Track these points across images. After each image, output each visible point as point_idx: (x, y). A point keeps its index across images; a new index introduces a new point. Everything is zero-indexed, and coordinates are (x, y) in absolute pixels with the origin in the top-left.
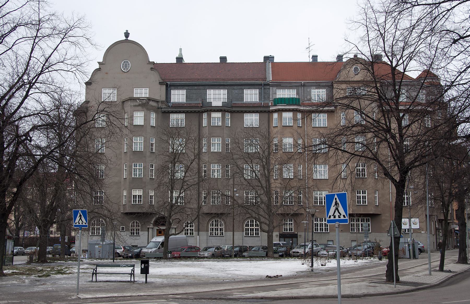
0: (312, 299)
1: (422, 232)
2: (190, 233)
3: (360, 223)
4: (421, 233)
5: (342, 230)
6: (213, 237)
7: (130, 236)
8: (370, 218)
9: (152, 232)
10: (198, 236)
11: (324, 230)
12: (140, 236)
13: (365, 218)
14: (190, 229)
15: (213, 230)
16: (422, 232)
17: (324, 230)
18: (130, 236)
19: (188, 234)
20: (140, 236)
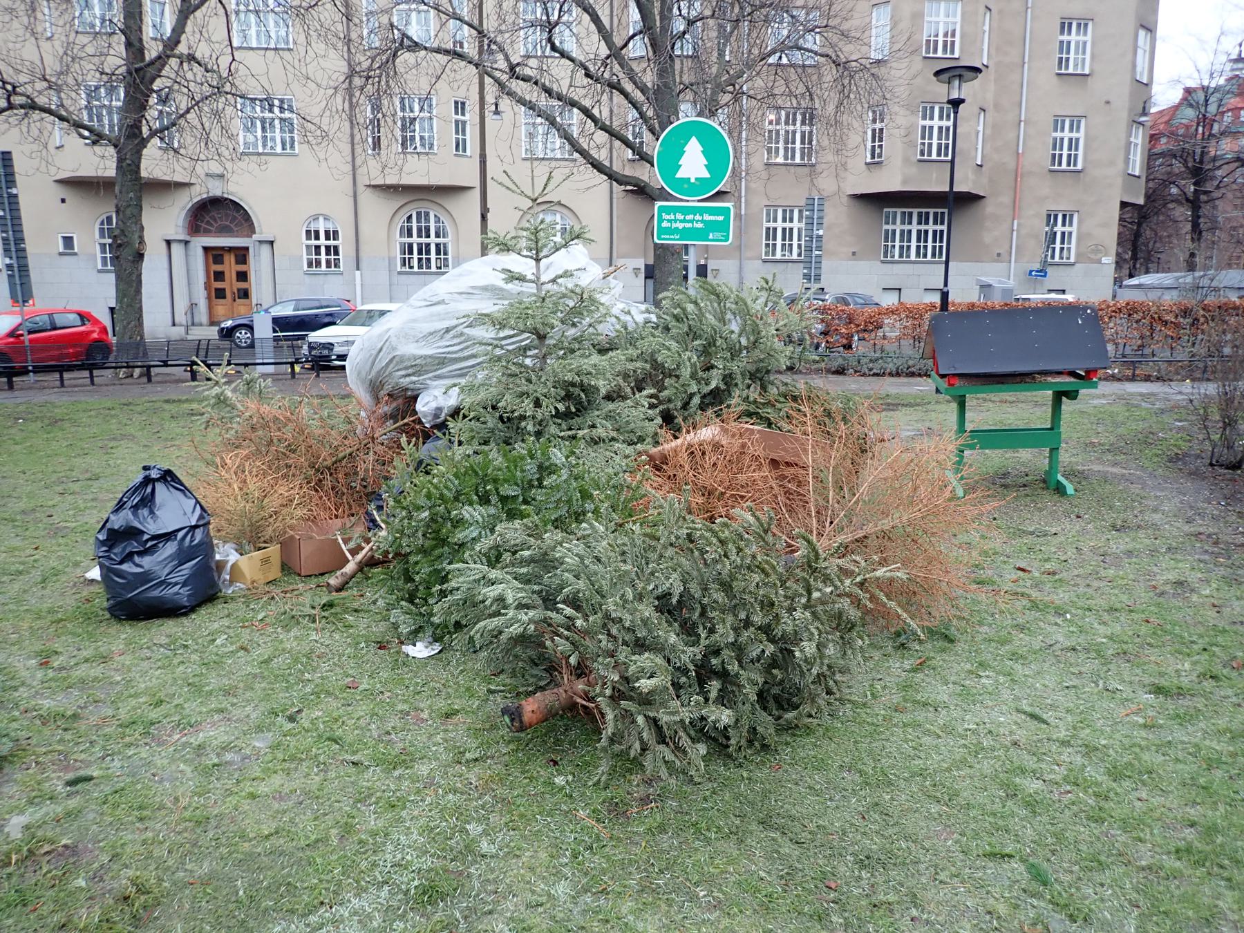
0: (203, 611)
1: (1104, 260)
2: (328, 262)
3: (914, 228)
4: (1099, 262)
5: (854, 254)
6: (411, 276)
7: (99, 271)
8: (946, 211)
9: (183, 257)
10: (358, 273)
11: (798, 155)
12: (76, 254)
13: (932, 211)
14: (328, 248)
15: (411, 252)
16: (1104, 260)
17: (798, 155)
18: (99, 271)
19: (318, 263)
20: (76, 254)
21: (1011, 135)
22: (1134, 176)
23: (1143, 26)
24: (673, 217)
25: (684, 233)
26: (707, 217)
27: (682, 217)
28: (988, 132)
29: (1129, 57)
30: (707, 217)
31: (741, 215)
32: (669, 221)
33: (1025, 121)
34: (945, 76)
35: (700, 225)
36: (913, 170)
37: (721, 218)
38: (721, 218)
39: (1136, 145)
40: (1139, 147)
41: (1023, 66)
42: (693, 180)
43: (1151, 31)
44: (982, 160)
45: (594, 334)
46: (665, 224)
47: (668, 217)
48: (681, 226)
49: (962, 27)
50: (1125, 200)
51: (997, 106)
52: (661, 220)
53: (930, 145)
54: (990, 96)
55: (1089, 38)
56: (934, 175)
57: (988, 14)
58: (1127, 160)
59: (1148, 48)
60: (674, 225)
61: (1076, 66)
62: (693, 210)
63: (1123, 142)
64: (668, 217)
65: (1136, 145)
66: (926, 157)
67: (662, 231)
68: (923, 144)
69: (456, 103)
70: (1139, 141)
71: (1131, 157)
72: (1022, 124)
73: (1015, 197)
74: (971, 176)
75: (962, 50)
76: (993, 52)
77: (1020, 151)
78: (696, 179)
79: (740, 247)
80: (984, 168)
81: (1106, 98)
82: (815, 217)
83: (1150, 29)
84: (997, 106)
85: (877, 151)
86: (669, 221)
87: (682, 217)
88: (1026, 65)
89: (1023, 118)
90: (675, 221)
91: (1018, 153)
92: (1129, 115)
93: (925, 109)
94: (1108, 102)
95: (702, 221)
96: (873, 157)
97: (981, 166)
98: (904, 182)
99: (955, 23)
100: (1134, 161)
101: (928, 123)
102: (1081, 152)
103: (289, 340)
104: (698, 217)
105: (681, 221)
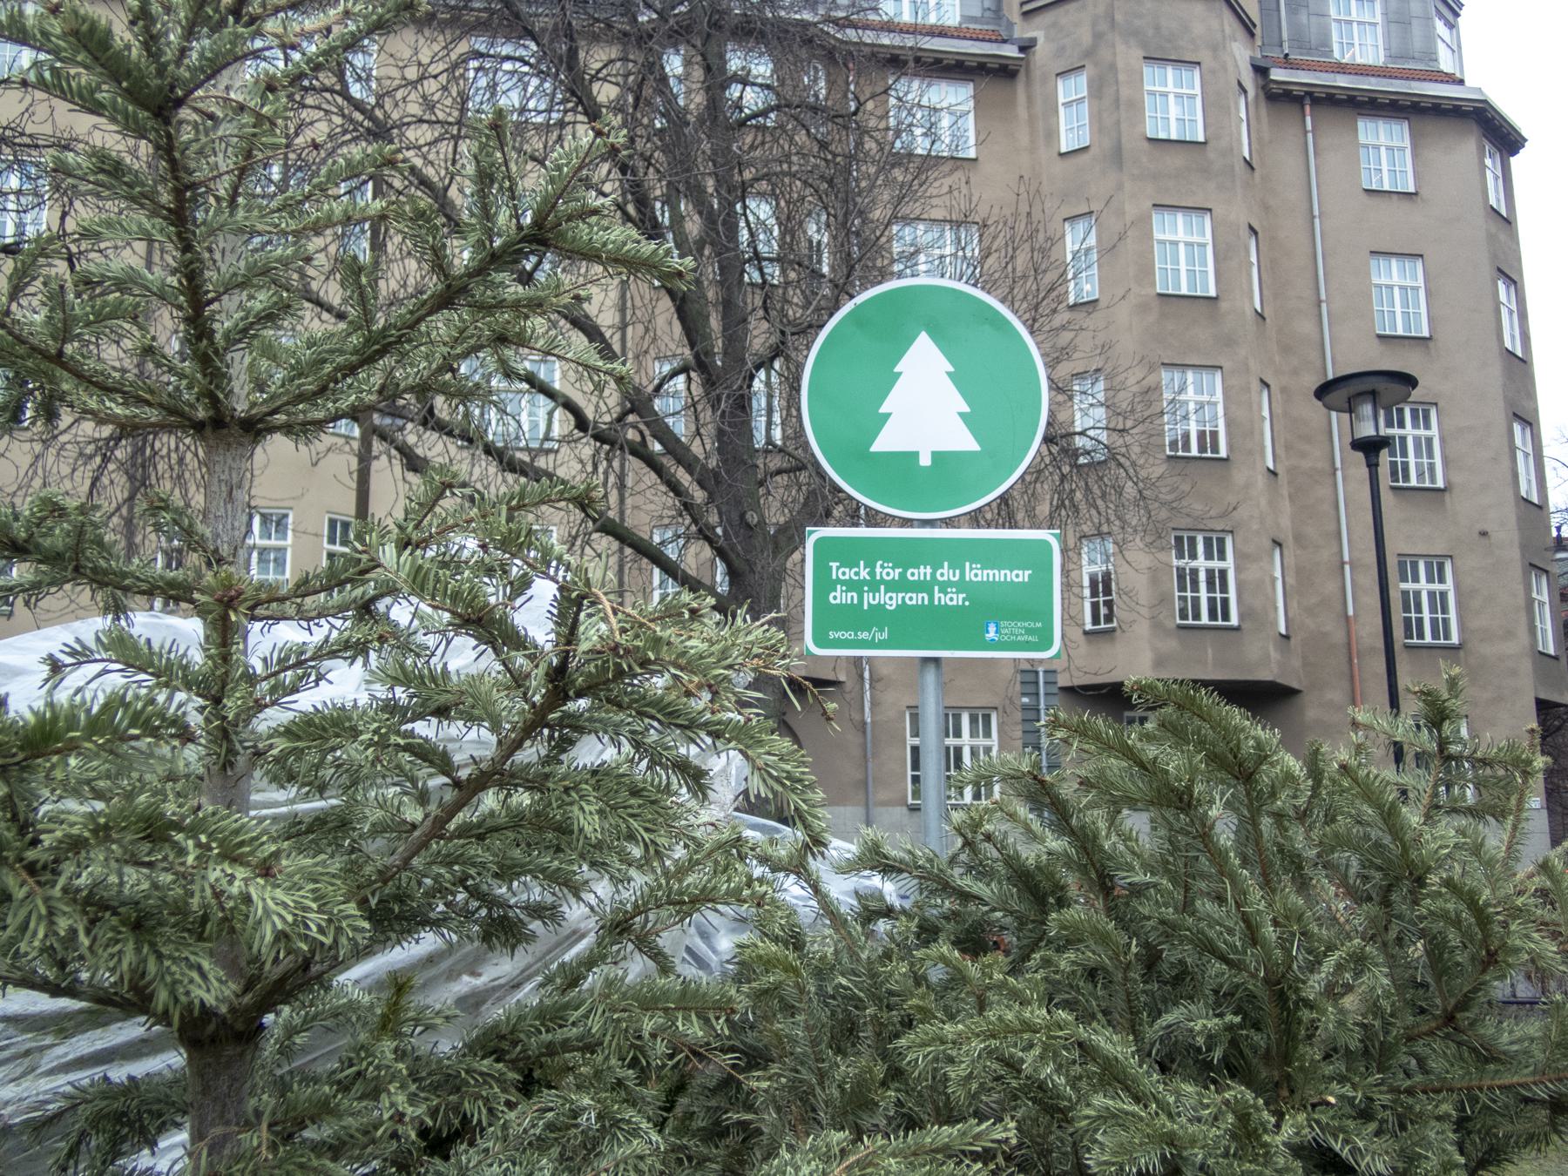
21: (1331, 587)
22: (1549, 656)
23: (1517, 417)
24: (864, 574)
25: (904, 625)
26: (976, 574)
27: (895, 574)
28: (1291, 580)
29: (1506, 463)
30: (976, 574)
31: (865, 723)
32: (851, 585)
33: (1351, 563)
34: (1340, 395)
35: (956, 599)
36: (1171, 645)
37: (1023, 576)
38: (1023, 576)
39: (1541, 604)
40: (1547, 608)
41: (1334, 474)
42: (925, 461)
43: (1530, 424)
44: (1287, 628)
45: (650, 1001)
46: (838, 597)
47: (848, 574)
48: (892, 601)
49: (1225, 408)
50: (1542, 696)
51: (1299, 539)
52: (825, 584)
53: (1196, 601)
54: (1285, 522)
55: (1434, 431)
56: (1210, 651)
57: (1265, 394)
58: (1532, 629)
59: (1529, 450)
60: (869, 599)
61: (1420, 476)
62: (933, 553)
63: (1521, 601)
64: (848, 574)
65: (1541, 604)
66: (1190, 622)
67: (829, 617)
68: (1183, 599)
69: (333, 523)
70: (1545, 597)
71: (1538, 623)
72: (1347, 568)
73: (1353, 691)
74: (1274, 655)
75: (1230, 447)
76: (1280, 452)
77: (1351, 612)
78: (936, 456)
79: (864, 784)
80: (1293, 641)
81: (1476, 535)
82: (1042, 706)
83: (1529, 422)
84: (1299, 539)
85: (1103, 611)
86: (851, 585)
87: (895, 574)
88: (1339, 474)
89: (1346, 558)
90: (874, 585)
91: (1347, 617)
92: (1523, 556)
93: (1179, 540)
94: (1484, 534)
95: (962, 586)
96: (1096, 620)
97: (1287, 637)
98: (1159, 662)
99: (1215, 404)
100: (1544, 631)
101: (1185, 562)
102: (1453, 615)
103: (568, 937)
104: (946, 573)
105: (892, 586)
